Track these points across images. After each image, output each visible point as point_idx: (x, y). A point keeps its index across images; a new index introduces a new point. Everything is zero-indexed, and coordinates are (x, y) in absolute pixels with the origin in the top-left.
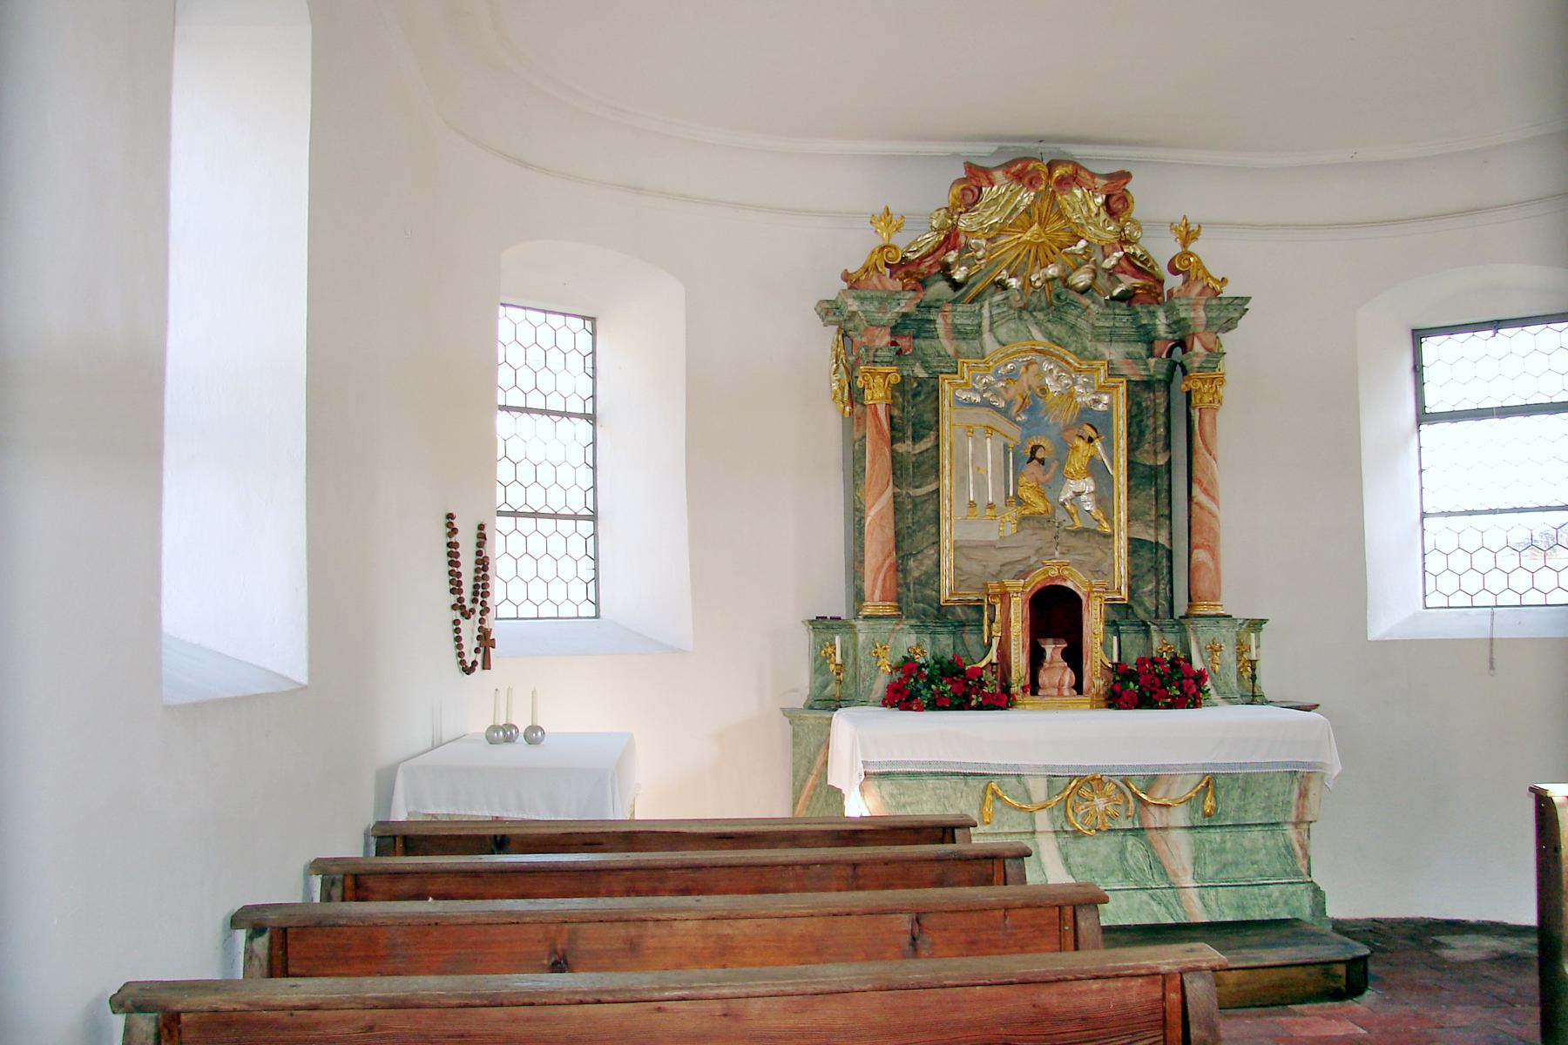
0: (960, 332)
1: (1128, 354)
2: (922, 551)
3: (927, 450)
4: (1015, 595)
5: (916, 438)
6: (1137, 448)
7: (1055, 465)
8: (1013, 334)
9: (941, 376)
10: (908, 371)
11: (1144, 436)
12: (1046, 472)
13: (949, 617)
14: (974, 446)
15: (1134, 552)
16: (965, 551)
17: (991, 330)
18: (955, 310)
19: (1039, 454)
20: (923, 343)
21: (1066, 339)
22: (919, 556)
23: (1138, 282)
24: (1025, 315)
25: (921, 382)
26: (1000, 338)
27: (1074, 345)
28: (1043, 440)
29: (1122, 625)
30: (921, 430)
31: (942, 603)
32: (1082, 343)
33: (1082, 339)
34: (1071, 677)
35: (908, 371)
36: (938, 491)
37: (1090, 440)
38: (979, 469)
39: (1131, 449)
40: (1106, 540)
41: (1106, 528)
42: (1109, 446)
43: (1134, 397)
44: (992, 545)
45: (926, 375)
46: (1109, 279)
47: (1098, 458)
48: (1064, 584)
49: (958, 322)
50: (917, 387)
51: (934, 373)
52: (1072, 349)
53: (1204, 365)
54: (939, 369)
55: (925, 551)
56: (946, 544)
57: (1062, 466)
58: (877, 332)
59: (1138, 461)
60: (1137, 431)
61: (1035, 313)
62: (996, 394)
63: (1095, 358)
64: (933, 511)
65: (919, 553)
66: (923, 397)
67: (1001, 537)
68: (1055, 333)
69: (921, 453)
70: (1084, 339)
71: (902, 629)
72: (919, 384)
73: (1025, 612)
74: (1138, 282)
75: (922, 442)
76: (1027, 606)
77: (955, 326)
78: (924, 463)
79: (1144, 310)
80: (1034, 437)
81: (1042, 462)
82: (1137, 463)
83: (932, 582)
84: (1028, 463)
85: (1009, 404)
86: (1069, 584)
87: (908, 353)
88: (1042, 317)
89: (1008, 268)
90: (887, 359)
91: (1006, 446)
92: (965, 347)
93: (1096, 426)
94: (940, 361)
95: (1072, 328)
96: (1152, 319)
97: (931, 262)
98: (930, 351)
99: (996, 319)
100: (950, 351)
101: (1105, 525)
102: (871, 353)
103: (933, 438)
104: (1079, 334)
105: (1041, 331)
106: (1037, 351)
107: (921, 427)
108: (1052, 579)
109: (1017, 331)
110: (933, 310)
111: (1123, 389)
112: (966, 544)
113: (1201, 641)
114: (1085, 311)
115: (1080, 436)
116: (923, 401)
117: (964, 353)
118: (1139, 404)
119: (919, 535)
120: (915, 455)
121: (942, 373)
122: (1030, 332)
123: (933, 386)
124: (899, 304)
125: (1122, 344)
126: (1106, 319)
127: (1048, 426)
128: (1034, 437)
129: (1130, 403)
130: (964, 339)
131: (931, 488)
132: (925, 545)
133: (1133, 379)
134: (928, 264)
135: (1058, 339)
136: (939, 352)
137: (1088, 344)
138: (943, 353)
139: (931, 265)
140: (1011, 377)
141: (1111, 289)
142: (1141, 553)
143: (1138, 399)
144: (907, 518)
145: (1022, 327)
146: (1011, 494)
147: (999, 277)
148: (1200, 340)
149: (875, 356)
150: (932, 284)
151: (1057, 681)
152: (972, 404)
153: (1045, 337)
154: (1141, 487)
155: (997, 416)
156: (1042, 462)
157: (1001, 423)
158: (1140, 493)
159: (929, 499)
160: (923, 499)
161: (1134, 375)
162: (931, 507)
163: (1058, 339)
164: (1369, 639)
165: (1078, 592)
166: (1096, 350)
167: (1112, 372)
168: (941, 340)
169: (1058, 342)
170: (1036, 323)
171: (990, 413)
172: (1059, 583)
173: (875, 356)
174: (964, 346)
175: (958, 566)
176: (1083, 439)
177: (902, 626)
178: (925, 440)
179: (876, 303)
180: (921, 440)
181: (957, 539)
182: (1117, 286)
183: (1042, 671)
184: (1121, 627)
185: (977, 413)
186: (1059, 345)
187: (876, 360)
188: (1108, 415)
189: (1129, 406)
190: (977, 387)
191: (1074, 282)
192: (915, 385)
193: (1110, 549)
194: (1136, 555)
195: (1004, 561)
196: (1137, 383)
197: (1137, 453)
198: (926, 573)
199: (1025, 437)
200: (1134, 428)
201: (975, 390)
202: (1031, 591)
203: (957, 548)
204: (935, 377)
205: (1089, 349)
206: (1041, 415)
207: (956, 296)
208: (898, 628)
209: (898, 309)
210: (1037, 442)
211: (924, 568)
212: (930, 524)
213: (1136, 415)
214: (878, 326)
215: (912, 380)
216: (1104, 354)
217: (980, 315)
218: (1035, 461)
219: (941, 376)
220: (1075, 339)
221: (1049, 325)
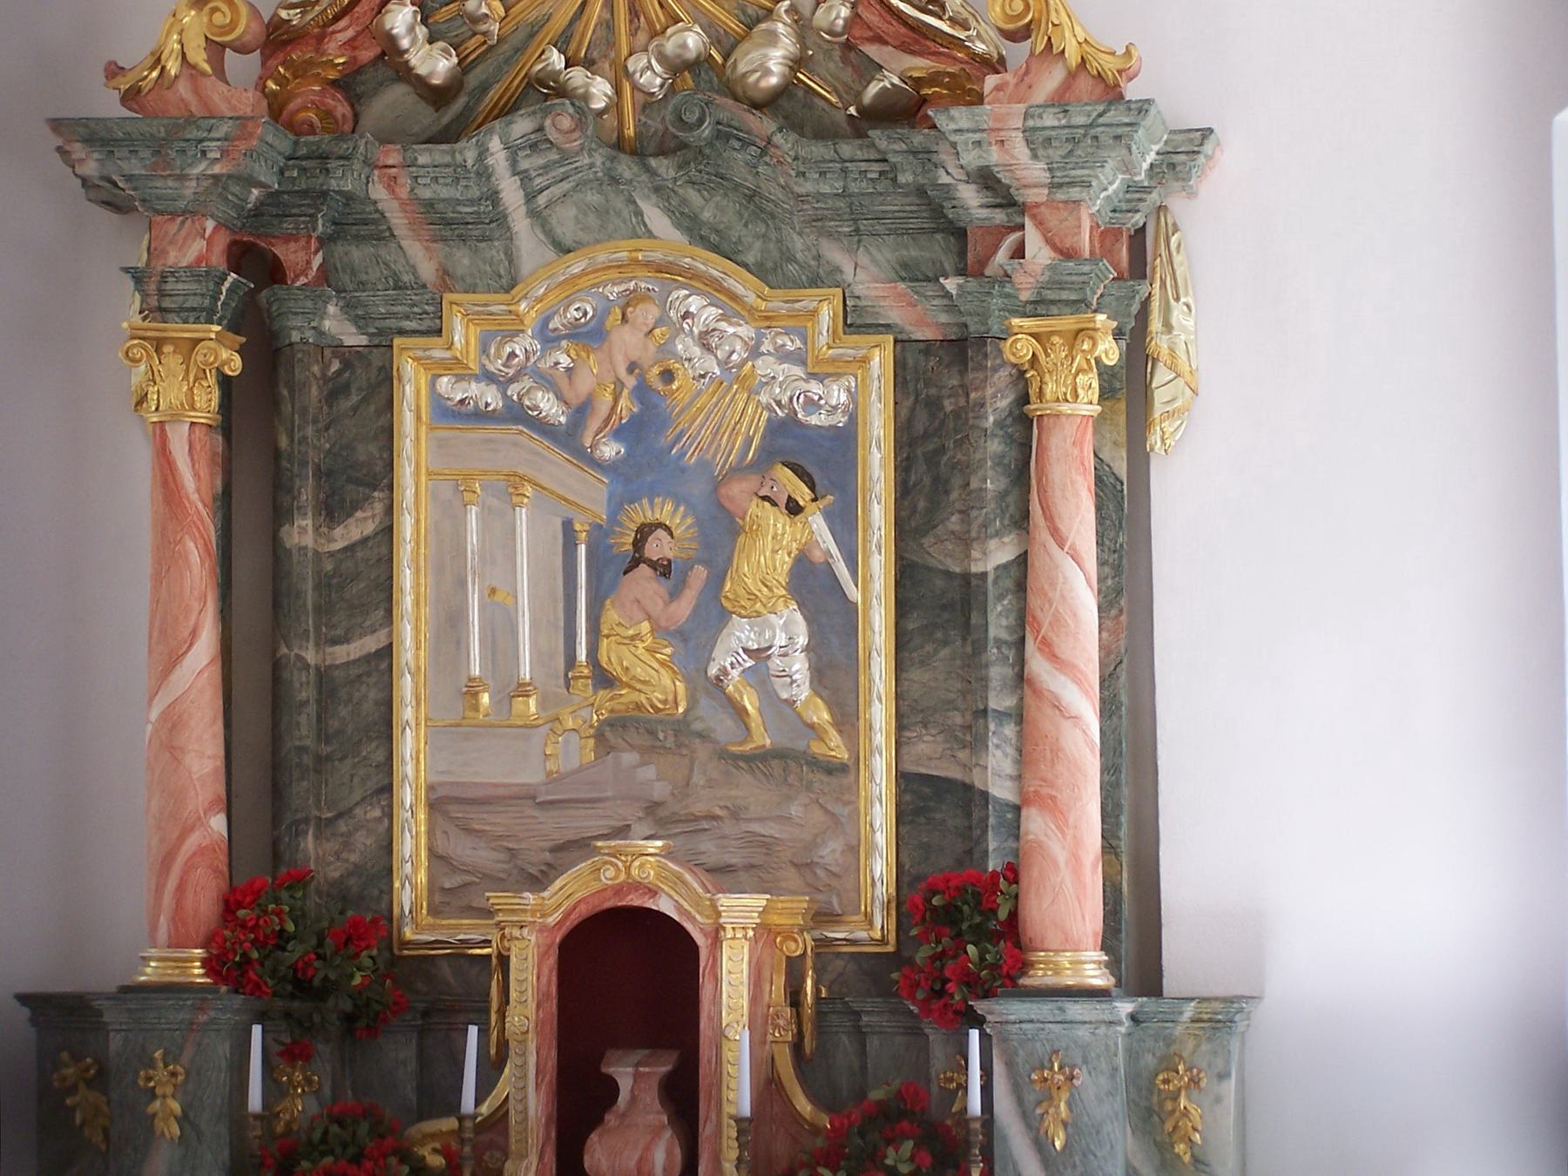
0: (448, 223)
1: (905, 266)
2: (351, 810)
3: (364, 541)
4: (516, 932)
5: (333, 511)
6: (929, 526)
7: (700, 574)
8: (592, 219)
9: (398, 342)
10: (299, 329)
11: (947, 492)
12: (674, 595)
13: (420, 986)
14: (484, 528)
15: (918, 811)
16: (455, 811)
17: (533, 213)
18: (413, 164)
19: (658, 547)
20: (358, 254)
21: (737, 231)
22: (342, 827)
23: (920, 65)
24: (626, 168)
25: (351, 358)
26: (559, 231)
27: (758, 245)
28: (669, 507)
29: (868, 1013)
30: (350, 487)
31: (396, 951)
32: (779, 241)
33: (778, 229)
34: (669, 1153)
35: (299, 329)
36: (387, 652)
37: (794, 508)
38: (493, 591)
39: (907, 529)
40: (834, 780)
41: (835, 747)
42: (845, 523)
43: (921, 385)
44: (527, 796)
45: (363, 340)
46: (845, 60)
47: (817, 556)
48: (650, 904)
49: (427, 194)
50: (339, 373)
51: (381, 332)
52: (750, 258)
53: (1051, 295)
54: (392, 323)
55: (358, 811)
56: (408, 795)
57: (717, 581)
58: (172, 228)
59: (932, 563)
60: (927, 480)
61: (653, 162)
62: (546, 381)
63: (815, 282)
64: (377, 703)
65: (340, 815)
66: (355, 399)
67: (549, 774)
68: (706, 215)
69: (350, 549)
70: (786, 229)
71: (213, 1021)
72: (347, 365)
73: (544, 980)
74: (920, 65)
75: (351, 520)
76: (552, 960)
77: (430, 205)
78: (355, 577)
79: (896, 147)
80: (645, 501)
81: (663, 569)
82: (929, 569)
83: (376, 892)
84: (625, 573)
85: (581, 412)
86: (665, 906)
87: (302, 280)
88: (672, 173)
89: (562, 43)
90: (193, 302)
91: (568, 526)
92: (466, 262)
93: (811, 469)
94: (394, 302)
95: (750, 198)
96: (925, 172)
97: (350, 33)
98: (374, 274)
99: (539, 182)
100: (427, 270)
101: (834, 738)
102: (152, 287)
103: (379, 507)
104: (773, 216)
105: (669, 211)
106: (647, 264)
107: (349, 480)
108: (636, 886)
109: (602, 212)
110: (332, 164)
111: (881, 360)
112: (458, 793)
113: (1019, 1060)
114: (764, 152)
115: (764, 498)
116: (355, 409)
117: (463, 279)
118: (933, 405)
119: (345, 768)
120: (331, 554)
121: (402, 332)
122: (639, 213)
123: (381, 369)
124: (204, 153)
125: (890, 240)
126: (822, 174)
127: (683, 470)
128: (645, 501)
129: (909, 402)
130: (463, 239)
131: (371, 644)
132: (357, 796)
133: (919, 335)
134: (343, 37)
135: (717, 231)
136: (396, 276)
137: (798, 244)
138: (406, 278)
139: (353, 39)
140: (589, 336)
141: (857, 87)
142: (938, 816)
143: (933, 391)
144: (298, 724)
145: (619, 203)
146: (582, 655)
147: (539, 67)
148: (1040, 224)
149: (162, 294)
150: (375, 92)
151: (632, 1164)
152: (481, 416)
153: (678, 225)
154: (939, 635)
155: (540, 444)
156: (663, 569)
157: (555, 468)
158: (936, 652)
159: (369, 675)
160: (354, 672)
161: (921, 322)
162: (373, 694)
163: (717, 231)
164: (470, 1026)
165: (688, 926)
166: (818, 257)
167: (855, 322)
168: (403, 243)
169: (714, 238)
170: (657, 190)
171: (523, 439)
172: (637, 903)
173: (162, 294)
174: (463, 260)
175: (440, 851)
176: (774, 504)
177: (213, 1014)
178: (359, 514)
179: (145, 153)
180: (350, 515)
181: (434, 779)
182: (873, 78)
183: (594, 1137)
184: (865, 1019)
185: (490, 441)
186: (716, 249)
187: (167, 303)
188: (844, 441)
189: (904, 413)
190: (492, 368)
191: (1074, 65)
192: (335, 366)
193: (846, 803)
194: (922, 820)
195: (560, 837)
196: (927, 347)
197: (927, 541)
198: (357, 869)
199: (618, 506)
200: (920, 472)
201: (489, 377)
202: (559, 924)
203: (439, 803)
204: (383, 343)
205: (799, 256)
206: (663, 442)
207: (445, 120)
208: (203, 1018)
209: (200, 168)
210: (650, 516)
211: (354, 858)
212: (370, 739)
213: (926, 436)
214: (174, 215)
215: (327, 352)
216: (838, 270)
217: (484, 173)
218: (644, 569)
219: (398, 342)
220: (762, 229)
221: (692, 194)
